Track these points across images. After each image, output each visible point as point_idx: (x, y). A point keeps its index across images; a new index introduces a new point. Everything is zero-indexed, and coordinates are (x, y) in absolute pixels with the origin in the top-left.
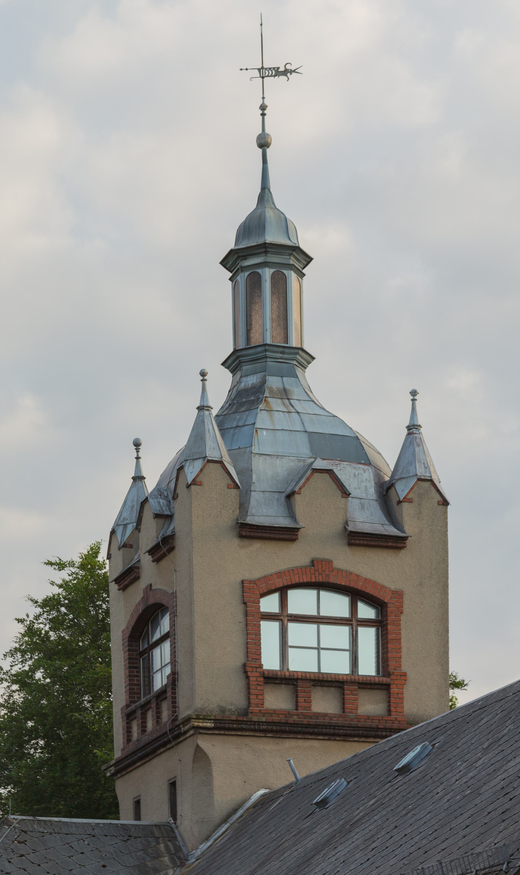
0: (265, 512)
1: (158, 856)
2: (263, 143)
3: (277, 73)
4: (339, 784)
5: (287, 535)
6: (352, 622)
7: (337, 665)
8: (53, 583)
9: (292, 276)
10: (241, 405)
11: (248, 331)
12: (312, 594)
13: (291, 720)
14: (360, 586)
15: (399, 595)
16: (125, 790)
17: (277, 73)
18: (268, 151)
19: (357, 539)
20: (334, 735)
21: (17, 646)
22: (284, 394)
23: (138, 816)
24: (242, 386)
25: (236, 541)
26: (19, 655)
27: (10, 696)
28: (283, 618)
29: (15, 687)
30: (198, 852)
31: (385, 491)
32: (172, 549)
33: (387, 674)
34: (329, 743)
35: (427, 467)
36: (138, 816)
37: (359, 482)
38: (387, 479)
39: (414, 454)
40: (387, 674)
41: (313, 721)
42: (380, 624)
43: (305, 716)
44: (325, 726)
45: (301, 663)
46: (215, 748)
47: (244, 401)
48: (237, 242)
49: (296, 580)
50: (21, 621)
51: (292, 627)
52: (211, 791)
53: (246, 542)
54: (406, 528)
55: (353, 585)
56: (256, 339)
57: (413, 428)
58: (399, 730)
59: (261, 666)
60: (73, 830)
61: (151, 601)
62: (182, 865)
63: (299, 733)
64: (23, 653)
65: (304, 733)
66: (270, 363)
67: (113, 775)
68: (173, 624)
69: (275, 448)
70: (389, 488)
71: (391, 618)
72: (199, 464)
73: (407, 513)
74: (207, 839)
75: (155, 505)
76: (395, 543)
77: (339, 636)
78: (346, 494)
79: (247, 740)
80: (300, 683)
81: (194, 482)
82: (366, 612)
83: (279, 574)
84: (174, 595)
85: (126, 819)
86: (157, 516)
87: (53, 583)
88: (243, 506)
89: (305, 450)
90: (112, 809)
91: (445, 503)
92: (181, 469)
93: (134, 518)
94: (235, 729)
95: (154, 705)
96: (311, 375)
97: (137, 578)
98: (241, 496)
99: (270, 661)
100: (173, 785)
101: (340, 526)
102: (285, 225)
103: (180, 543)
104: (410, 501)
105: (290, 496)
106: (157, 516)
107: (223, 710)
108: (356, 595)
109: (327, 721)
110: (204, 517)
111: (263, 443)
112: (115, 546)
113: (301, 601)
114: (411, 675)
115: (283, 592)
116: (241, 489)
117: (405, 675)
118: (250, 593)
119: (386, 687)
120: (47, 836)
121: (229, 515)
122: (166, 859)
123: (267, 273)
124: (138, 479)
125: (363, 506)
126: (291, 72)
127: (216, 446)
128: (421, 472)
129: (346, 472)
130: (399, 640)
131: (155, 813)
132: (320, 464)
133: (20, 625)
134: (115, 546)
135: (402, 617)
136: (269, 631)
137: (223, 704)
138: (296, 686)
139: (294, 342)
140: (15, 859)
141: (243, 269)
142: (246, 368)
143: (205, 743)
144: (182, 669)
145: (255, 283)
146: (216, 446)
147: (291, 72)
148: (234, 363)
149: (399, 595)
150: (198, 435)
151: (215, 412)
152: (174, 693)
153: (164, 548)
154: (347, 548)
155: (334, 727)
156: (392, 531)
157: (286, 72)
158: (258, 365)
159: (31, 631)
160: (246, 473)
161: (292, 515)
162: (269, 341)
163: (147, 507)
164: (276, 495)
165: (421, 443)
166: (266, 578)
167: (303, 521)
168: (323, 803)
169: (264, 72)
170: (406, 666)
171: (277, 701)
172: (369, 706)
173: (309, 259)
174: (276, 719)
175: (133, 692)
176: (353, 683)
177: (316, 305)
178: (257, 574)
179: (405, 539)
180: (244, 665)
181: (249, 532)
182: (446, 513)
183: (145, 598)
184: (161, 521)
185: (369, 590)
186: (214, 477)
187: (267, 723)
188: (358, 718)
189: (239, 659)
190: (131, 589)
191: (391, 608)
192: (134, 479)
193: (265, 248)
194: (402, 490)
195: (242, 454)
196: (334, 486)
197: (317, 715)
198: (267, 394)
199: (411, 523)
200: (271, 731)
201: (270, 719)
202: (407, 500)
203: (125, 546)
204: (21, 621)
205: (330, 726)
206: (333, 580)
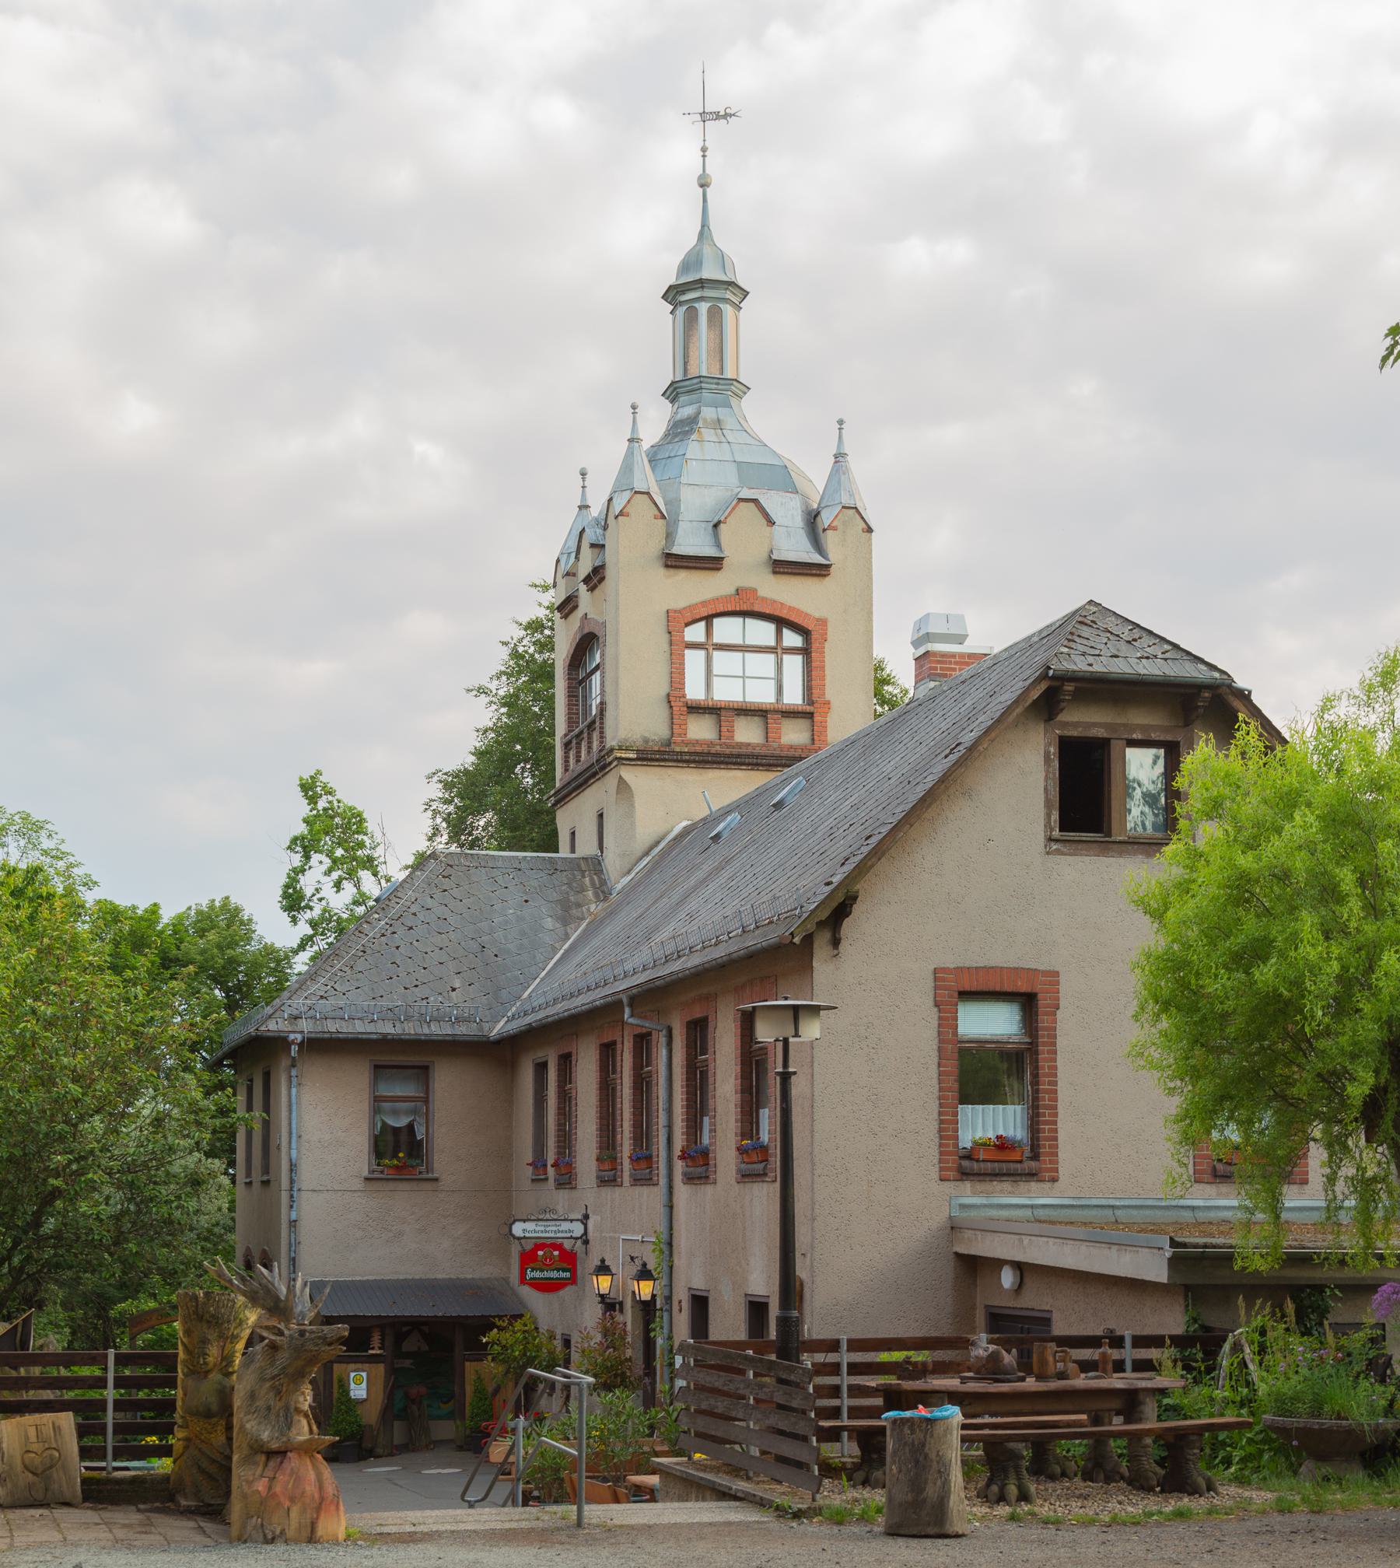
0: (691, 543)
1: (582, 890)
2: (704, 184)
3: (717, 116)
4: (734, 818)
5: (712, 564)
6: (777, 650)
7: (762, 694)
8: (540, 605)
9: (728, 309)
10: (676, 435)
11: (686, 363)
12: (737, 621)
13: (713, 750)
14: (784, 614)
15: (823, 622)
16: (564, 819)
17: (717, 116)
18: (708, 190)
19: (782, 567)
20: (757, 764)
21: (503, 669)
22: (718, 424)
23: (573, 851)
24: (679, 417)
25: (662, 571)
26: (504, 678)
27: (499, 719)
28: (706, 646)
29: (504, 710)
30: (619, 887)
31: (812, 519)
32: (602, 579)
33: (811, 702)
34: (752, 773)
35: (851, 495)
36: (573, 851)
37: (787, 511)
38: (815, 506)
39: (839, 483)
40: (811, 702)
41: (735, 751)
42: (805, 651)
43: (728, 746)
44: (748, 756)
45: (726, 692)
46: (638, 778)
47: (680, 430)
48: (679, 275)
49: (721, 608)
50: (505, 644)
51: (717, 655)
52: (633, 824)
53: (672, 571)
54: (830, 556)
55: (777, 613)
56: (693, 372)
57: (839, 457)
58: (801, 759)
59: (684, 696)
60: (500, 864)
61: (586, 631)
62: (606, 899)
63: (722, 763)
64: (509, 675)
65: (727, 763)
66: (705, 395)
67: (554, 805)
68: (602, 655)
69: (704, 482)
70: (816, 516)
71: (815, 645)
72: (627, 495)
73: (831, 540)
74: (629, 872)
75: (590, 536)
76: (820, 571)
77: (765, 664)
78: (771, 523)
79: (670, 771)
80: (723, 713)
81: (621, 513)
82: (792, 639)
83: (704, 604)
84: (604, 624)
85: (564, 852)
86: (593, 546)
87: (540, 605)
88: (670, 536)
89: (733, 479)
90: (550, 843)
91: (870, 530)
92: (610, 500)
93: (574, 549)
94: (657, 760)
95: (585, 735)
96: (748, 405)
97: (576, 607)
98: (668, 525)
99: (694, 691)
100: (601, 816)
101: (765, 555)
102: (722, 260)
103: (609, 573)
104: (835, 529)
105: (716, 526)
106: (593, 546)
107: (646, 741)
108: (781, 622)
109: (750, 750)
110: (632, 549)
111: (692, 472)
112: (559, 575)
113: (727, 629)
114: (834, 705)
115: (708, 619)
116: (668, 520)
117: (829, 703)
118: (676, 621)
119: (809, 716)
120: (473, 870)
121: (656, 545)
122: (590, 893)
123: (703, 308)
124: (583, 507)
125: (789, 534)
126: (731, 115)
127: (645, 478)
128: (846, 500)
129: (773, 502)
130: (823, 668)
131: (587, 847)
132: (746, 493)
133: (505, 648)
134: (559, 575)
135: (827, 644)
136: (694, 661)
137: (647, 735)
138: (719, 715)
139: (729, 374)
140: (438, 895)
141: (681, 303)
142: (683, 399)
143: (628, 774)
144: (609, 699)
145: (691, 318)
146: (645, 478)
147: (731, 115)
148: (673, 392)
149: (823, 622)
150: (627, 467)
151: (646, 445)
152: (602, 724)
153: (596, 578)
154: (772, 576)
155: (757, 757)
156: (817, 559)
157: (726, 116)
158: (694, 397)
159: (515, 655)
160: (674, 503)
161: (718, 545)
162: (704, 374)
163: (585, 536)
164: (703, 525)
165: (847, 471)
166: (691, 608)
167: (728, 552)
168: (717, 837)
169: (705, 116)
170: (829, 695)
171: (700, 730)
172: (793, 735)
173: (746, 294)
174: (698, 749)
175: (571, 722)
176: (776, 711)
177: (758, 333)
178: (681, 604)
179: (828, 566)
180: (668, 695)
181: (674, 561)
182: (870, 539)
183: (581, 628)
184: (596, 550)
185: (793, 618)
186: (641, 509)
187: (690, 753)
188: (781, 747)
189: (664, 689)
190: (571, 617)
191: (815, 636)
192: (580, 507)
193: (701, 283)
194: (826, 518)
195: (669, 484)
196: (759, 515)
197: (741, 745)
198: (700, 424)
199: (836, 549)
200: (694, 762)
201: (692, 749)
202: (830, 527)
203: (568, 574)
204: (505, 644)
205: (753, 756)
206: (757, 608)
